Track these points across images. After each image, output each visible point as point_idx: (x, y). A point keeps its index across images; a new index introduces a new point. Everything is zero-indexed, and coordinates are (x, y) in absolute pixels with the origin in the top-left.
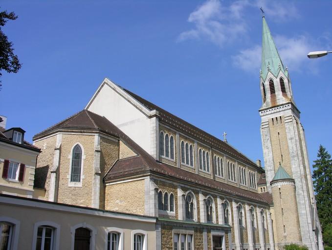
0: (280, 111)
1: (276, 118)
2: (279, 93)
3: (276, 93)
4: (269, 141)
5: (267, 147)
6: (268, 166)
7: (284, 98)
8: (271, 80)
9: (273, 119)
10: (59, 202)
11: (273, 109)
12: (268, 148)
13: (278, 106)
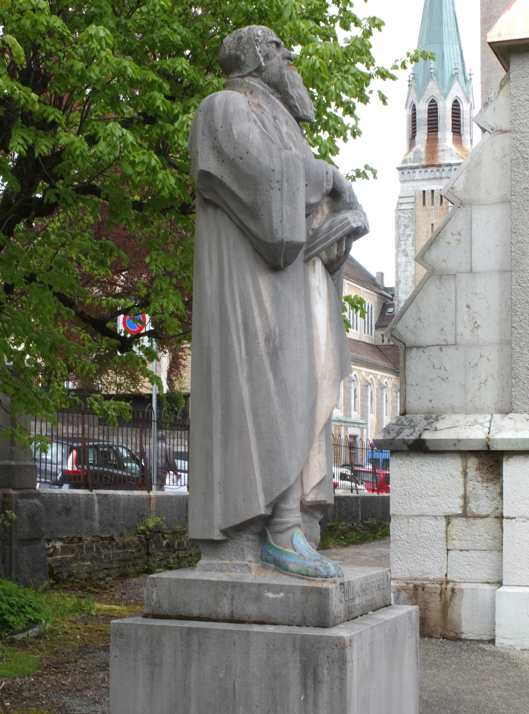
0: (441, 178)
1: (433, 191)
2: (446, 136)
3: (440, 135)
4: (410, 239)
5: (405, 251)
6: (402, 293)
7: (455, 149)
8: (433, 101)
9: (424, 192)
10: (439, 347)
11: (429, 170)
12: (406, 255)
13: (440, 166)
